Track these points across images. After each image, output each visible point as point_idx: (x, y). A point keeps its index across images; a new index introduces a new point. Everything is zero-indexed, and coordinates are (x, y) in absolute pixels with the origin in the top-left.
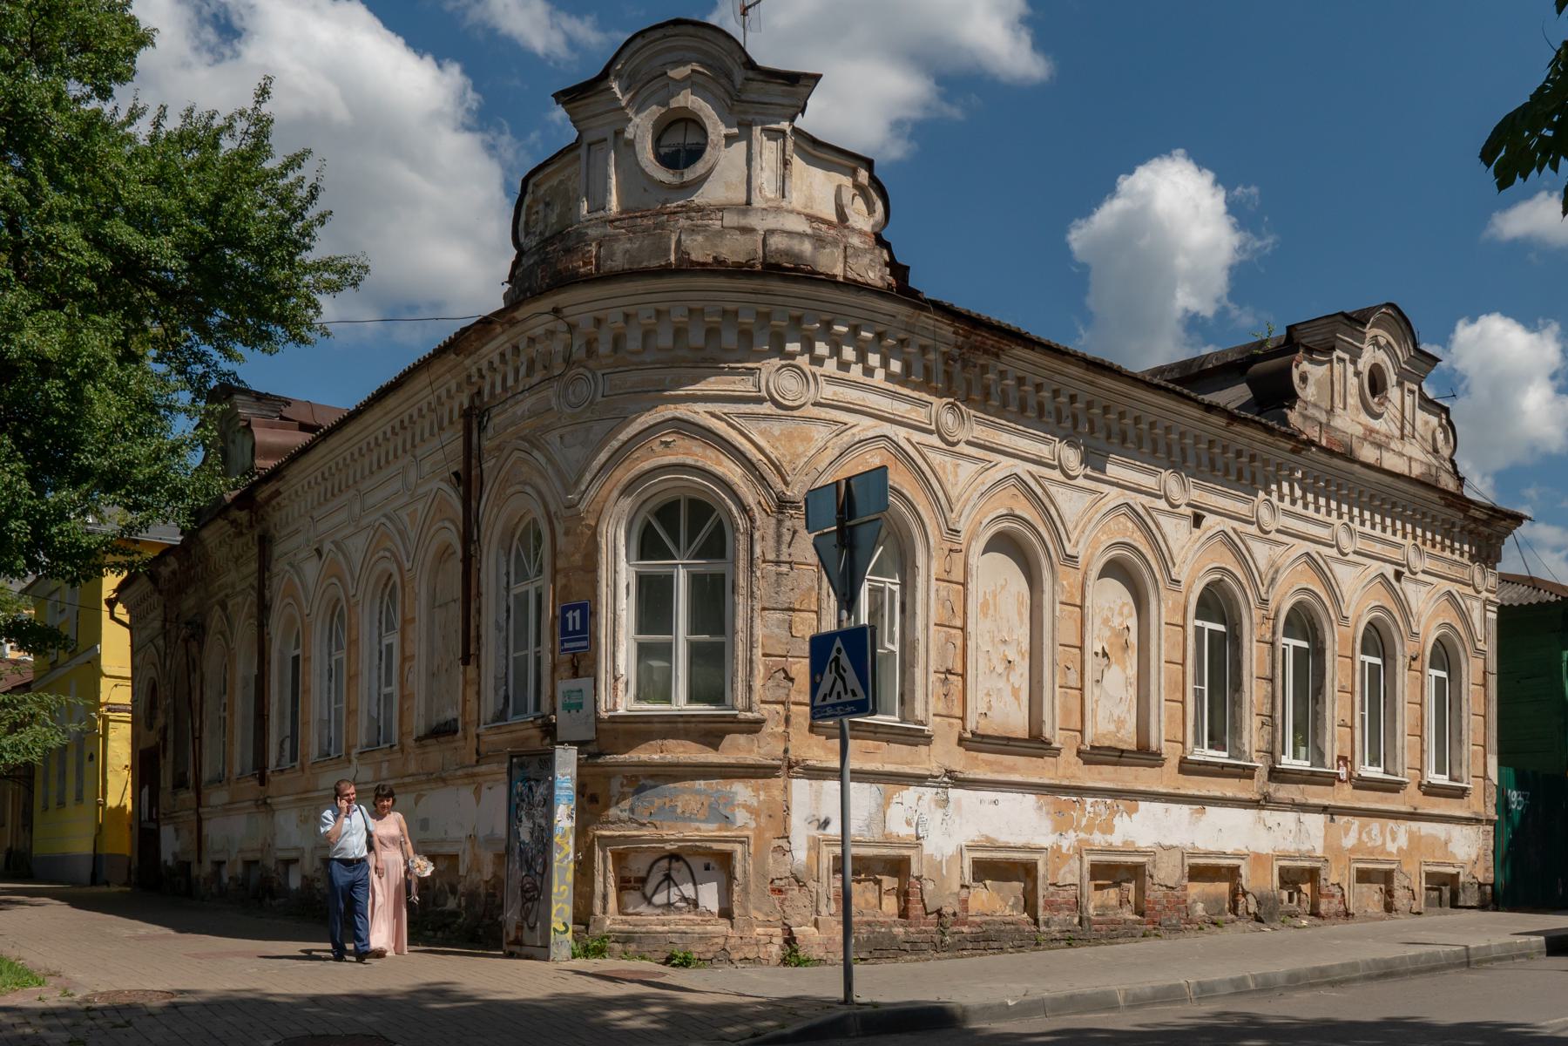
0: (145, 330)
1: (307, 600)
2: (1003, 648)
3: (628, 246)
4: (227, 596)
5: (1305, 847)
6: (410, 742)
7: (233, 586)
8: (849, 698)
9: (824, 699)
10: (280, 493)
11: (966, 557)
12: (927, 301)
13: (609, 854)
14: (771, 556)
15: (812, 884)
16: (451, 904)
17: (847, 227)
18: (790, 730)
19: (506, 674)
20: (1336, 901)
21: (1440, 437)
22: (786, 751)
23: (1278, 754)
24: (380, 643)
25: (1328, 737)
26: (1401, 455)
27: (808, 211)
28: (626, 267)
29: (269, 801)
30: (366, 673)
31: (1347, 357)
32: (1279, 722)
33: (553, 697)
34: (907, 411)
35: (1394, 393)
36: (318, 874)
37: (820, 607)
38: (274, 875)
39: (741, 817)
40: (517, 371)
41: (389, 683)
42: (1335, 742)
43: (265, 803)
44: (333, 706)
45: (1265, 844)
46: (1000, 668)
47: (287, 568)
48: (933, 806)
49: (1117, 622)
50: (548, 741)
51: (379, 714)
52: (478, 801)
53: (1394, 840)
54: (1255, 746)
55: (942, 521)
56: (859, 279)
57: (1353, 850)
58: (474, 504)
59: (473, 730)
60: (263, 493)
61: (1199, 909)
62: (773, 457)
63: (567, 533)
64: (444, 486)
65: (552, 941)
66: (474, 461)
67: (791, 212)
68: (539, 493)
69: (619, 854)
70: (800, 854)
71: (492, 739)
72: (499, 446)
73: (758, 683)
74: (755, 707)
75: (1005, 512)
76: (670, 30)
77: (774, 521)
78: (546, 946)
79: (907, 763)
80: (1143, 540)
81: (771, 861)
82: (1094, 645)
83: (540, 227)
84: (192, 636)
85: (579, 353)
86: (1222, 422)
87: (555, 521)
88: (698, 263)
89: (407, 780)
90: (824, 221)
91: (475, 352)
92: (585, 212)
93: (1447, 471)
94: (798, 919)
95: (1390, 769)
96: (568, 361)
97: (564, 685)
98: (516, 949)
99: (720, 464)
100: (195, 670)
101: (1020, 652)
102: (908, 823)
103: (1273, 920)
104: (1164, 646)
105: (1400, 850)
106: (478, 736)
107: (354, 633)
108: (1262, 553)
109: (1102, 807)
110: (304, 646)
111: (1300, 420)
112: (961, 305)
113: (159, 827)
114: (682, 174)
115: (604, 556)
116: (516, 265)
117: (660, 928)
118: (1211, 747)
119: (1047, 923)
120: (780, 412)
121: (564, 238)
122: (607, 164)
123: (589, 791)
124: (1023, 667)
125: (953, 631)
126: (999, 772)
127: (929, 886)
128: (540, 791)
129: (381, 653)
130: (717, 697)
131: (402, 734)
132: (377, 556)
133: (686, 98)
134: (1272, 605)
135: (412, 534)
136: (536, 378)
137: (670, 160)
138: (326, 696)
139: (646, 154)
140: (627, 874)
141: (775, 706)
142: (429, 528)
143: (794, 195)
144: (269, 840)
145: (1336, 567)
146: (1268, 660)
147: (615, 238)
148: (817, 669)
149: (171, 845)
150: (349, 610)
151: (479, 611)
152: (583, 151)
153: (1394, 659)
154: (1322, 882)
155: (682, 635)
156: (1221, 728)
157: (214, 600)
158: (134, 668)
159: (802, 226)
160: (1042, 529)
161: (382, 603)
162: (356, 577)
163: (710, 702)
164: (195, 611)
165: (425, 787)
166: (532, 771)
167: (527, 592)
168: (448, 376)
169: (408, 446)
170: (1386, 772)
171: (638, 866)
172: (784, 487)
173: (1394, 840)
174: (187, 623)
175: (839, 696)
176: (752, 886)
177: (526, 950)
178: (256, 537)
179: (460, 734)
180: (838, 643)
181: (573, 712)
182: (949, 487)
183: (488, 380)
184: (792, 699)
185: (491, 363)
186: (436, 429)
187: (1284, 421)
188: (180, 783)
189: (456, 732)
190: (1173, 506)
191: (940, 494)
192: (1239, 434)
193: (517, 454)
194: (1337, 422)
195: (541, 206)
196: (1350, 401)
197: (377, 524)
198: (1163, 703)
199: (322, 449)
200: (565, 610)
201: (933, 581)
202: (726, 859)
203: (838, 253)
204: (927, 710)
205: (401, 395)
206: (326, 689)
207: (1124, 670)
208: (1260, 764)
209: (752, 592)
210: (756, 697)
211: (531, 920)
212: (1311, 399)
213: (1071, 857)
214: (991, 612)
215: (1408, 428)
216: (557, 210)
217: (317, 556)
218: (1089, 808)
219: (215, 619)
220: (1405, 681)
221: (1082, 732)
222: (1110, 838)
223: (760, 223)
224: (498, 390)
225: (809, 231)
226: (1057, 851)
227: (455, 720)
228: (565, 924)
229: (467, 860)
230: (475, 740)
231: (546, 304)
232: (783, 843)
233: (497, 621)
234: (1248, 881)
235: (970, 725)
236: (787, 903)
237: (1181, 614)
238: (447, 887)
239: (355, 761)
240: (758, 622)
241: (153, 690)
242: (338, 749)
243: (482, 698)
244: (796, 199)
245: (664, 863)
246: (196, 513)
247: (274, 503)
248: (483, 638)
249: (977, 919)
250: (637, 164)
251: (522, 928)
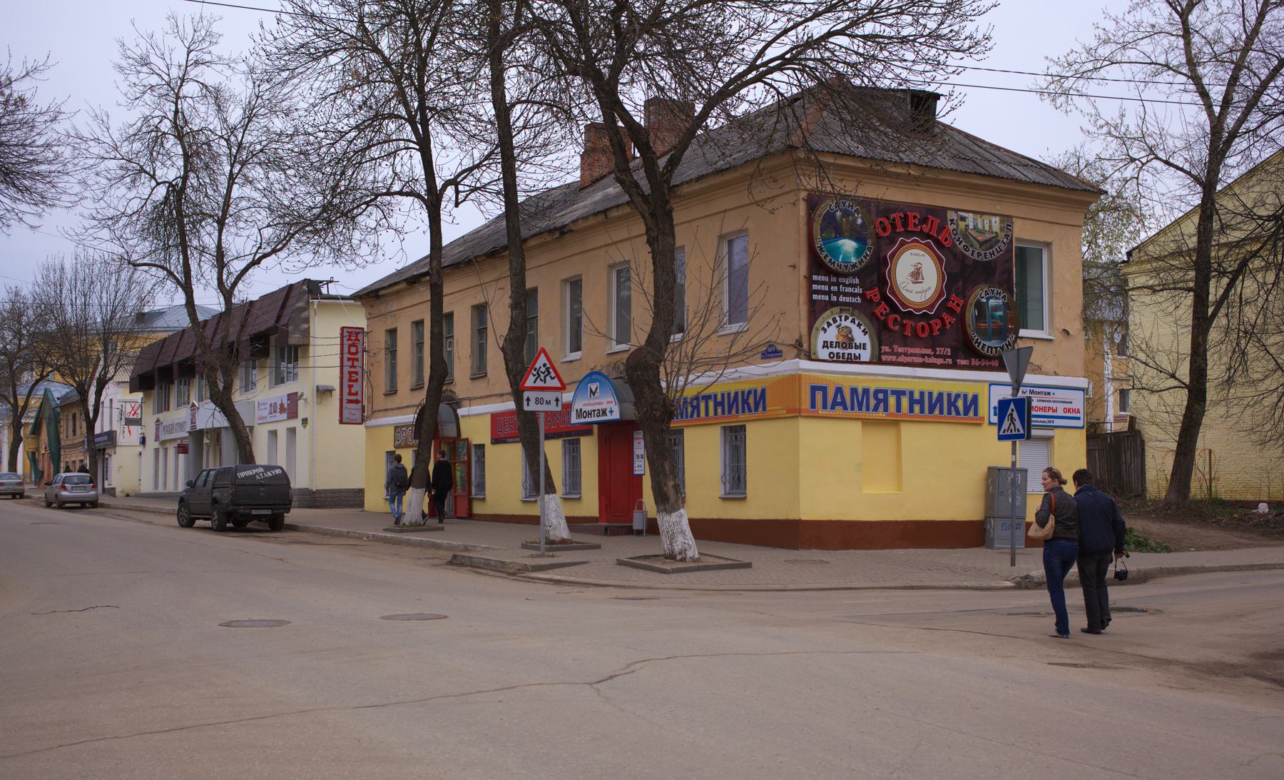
180: (1012, 406)
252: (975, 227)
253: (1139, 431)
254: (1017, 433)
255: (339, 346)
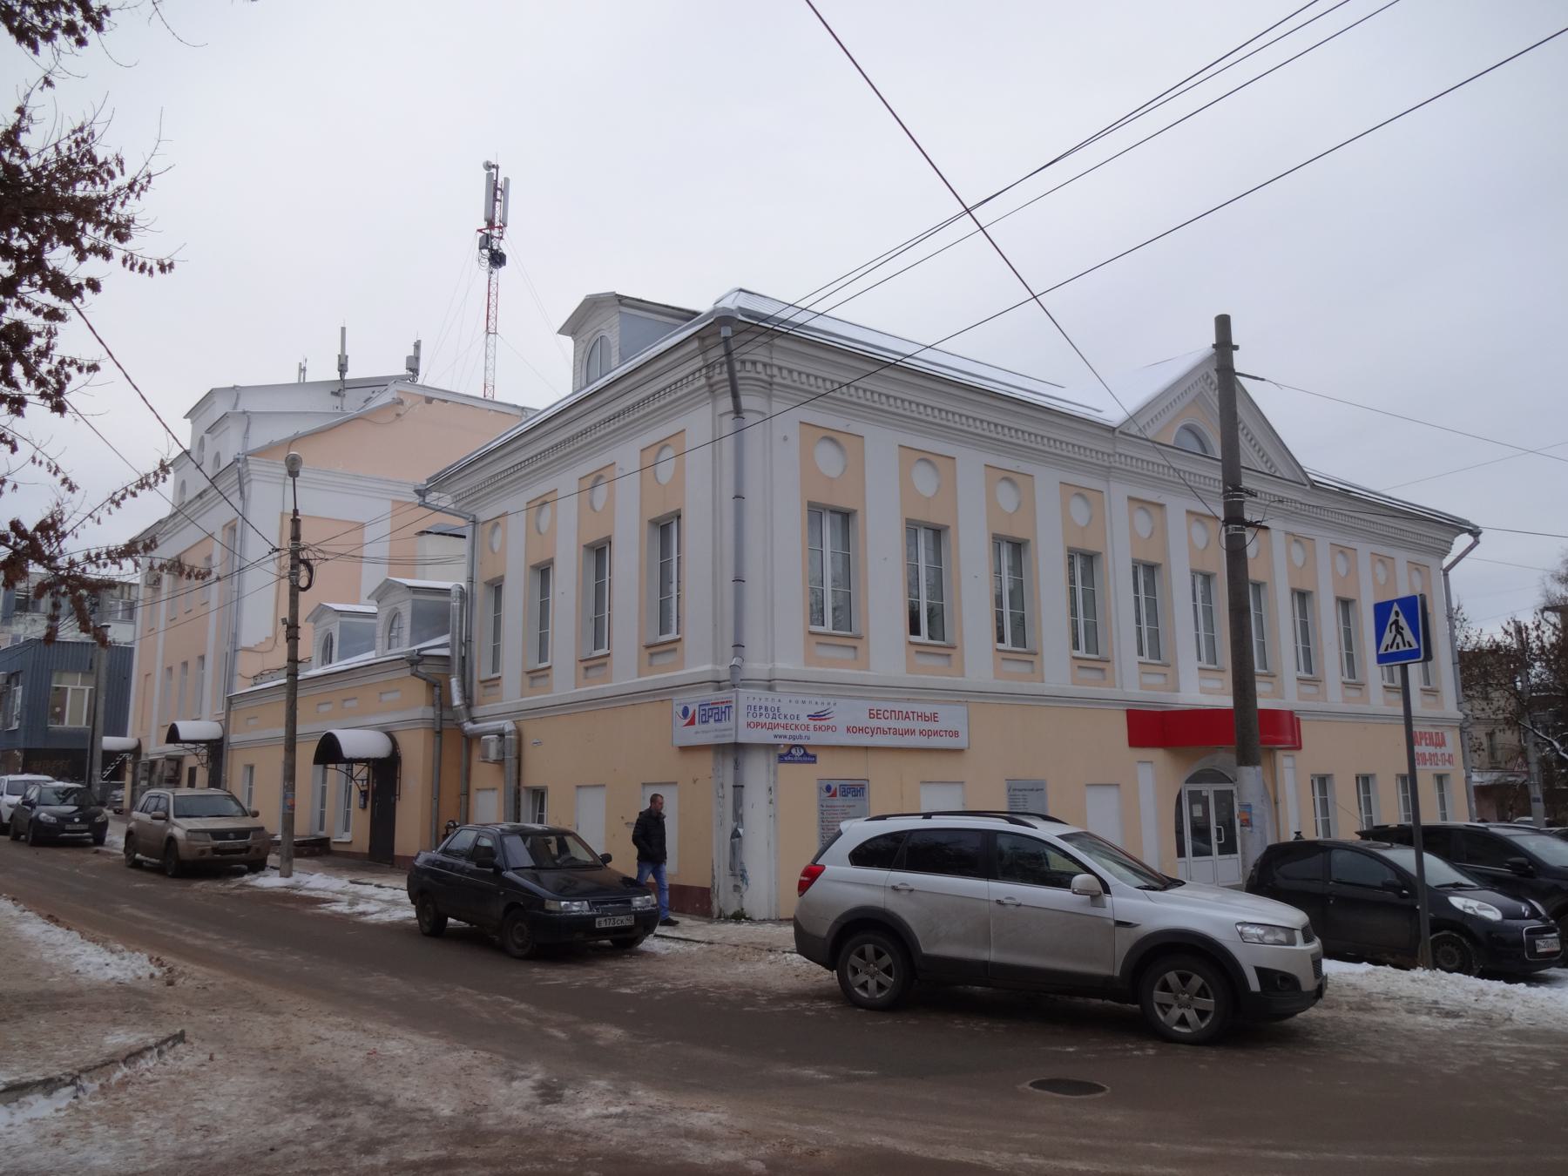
9: (1386, 650)
175: (1398, 647)
180: (1396, 607)
252: (716, 1145)
253: (937, 843)
254: (1407, 648)
255: (299, 731)
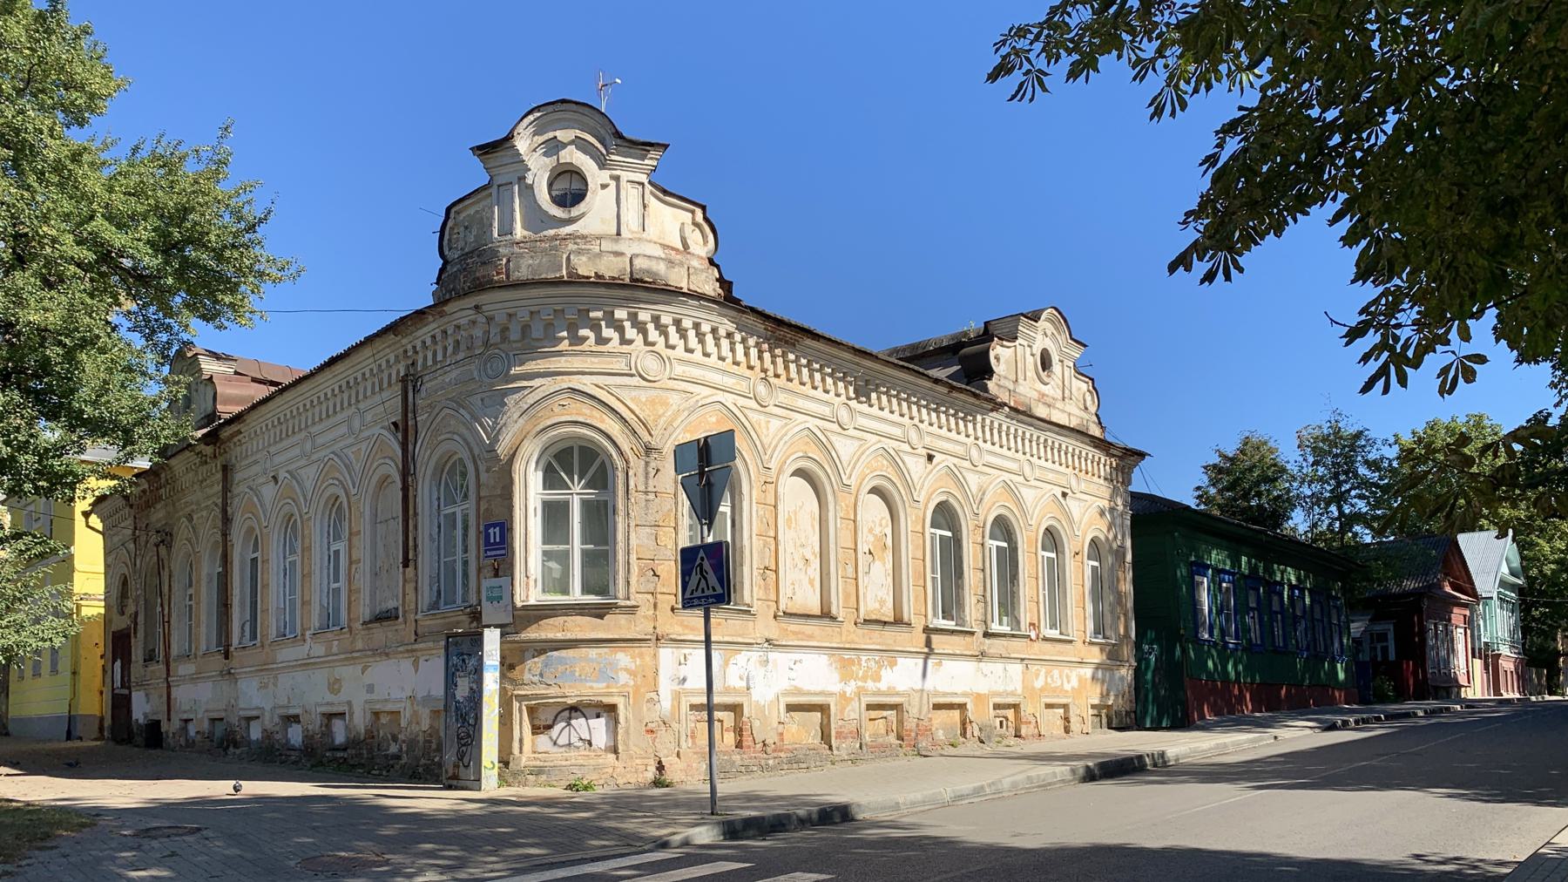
0: (119, 305)
1: (265, 516)
2: (801, 550)
3: (531, 262)
4: (193, 511)
5: (1010, 688)
6: (357, 626)
7: (198, 504)
8: (711, 592)
9: (692, 593)
10: (241, 433)
11: (776, 486)
12: (746, 307)
13: (524, 708)
14: (641, 488)
15: (675, 725)
16: (393, 749)
17: (689, 253)
18: (658, 613)
19: (438, 574)
20: (1032, 726)
21: (1088, 398)
22: (655, 628)
23: (989, 622)
24: (329, 549)
25: (1022, 609)
26: (1064, 411)
27: (660, 241)
28: (530, 277)
29: (232, 671)
30: (318, 572)
31: (1025, 343)
32: (989, 599)
33: (479, 592)
34: (734, 384)
35: (1056, 367)
36: (277, 728)
37: (676, 524)
38: (237, 729)
39: (623, 678)
40: (445, 349)
41: (337, 580)
42: (1026, 614)
43: (230, 673)
44: (288, 597)
45: (983, 687)
46: (801, 564)
47: (247, 490)
48: (758, 665)
49: (877, 530)
50: (475, 624)
51: (328, 604)
52: (416, 671)
53: (1069, 682)
54: (974, 618)
55: (759, 461)
56: (699, 291)
57: (1042, 690)
58: (410, 447)
59: (412, 617)
60: (225, 433)
61: (940, 735)
62: (641, 417)
63: (488, 471)
64: (385, 433)
65: (483, 775)
66: (410, 415)
67: (650, 241)
68: (465, 440)
69: (532, 708)
70: (666, 703)
71: (427, 623)
72: (430, 405)
73: (633, 580)
74: (632, 597)
75: (801, 454)
76: (559, 107)
77: (643, 463)
78: (479, 780)
79: (740, 636)
80: (893, 472)
81: (645, 709)
82: (863, 547)
83: (461, 244)
84: (162, 541)
85: (495, 338)
86: (945, 390)
87: (479, 463)
88: (584, 277)
89: (355, 655)
90: (673, 249)
91: (411, 334)
92: (496, 236)
93: (1094, 422)
94: (666, 751)
95: (1063, 631)
96: (487, 344)
97: (487, 583)
98: (454, 782)
99: (603, 421)
100: (163, 568)
101: (814, 553)
102: (741, 678)
103: (990, 742)
104: (909, 550)
105: (1073, 688)
106: (416, 621)
107: (307, 541)
108: (973, 481)
109: (873, 663)
110: (262, 550)
111: (996, 387)
112: (769, 311)
113: (130, 693)
114: (570, 211)
115: (518, 487)
116: (442, 271)
117: (564, 763)
118: (943, 618)
119: (838, 749)
120: (645, 383)
121: (483, 254)
122: (513, 201)
123: (508, 662)
124: (816, 563)
125: (768, 539)
126: (802, 640)
127: (756, 724)
128: (472, 663)
129: (329, 556)
130: (603, 591)
131: (350, 620)
132: (324, 485)
133: (571, 154)
134: (981, 518)
135: (357, 467)
136: (461, 355)
137: (562, 201)
138: (282, 589)
139: (543, 196)
140: (537, 722)
141: (646, 595)
142: (371, 464)
143: (652, 229)
144: (233, 701)
145: (1022, 489)
146: (980, 556)
147: (521, 256)
148: (686, 574)
149: (141, 709)
150: (302, 522)
151: (416, 527)
152: (494, 190)
153: (1063, 553)
154: (1022, 713)
155: (577, 545)
156: (951, 604)
157: (181, 513)
158: (107, 566)
159: (658, 252)
160: (827, 467)
161: (330, 518)
162: (308, 498)
163: (597, 594)
164: (163, 522)
165: (371, 660)
166: (465, 648)
167: (454, 513)
168: (388, 350)
169: (353, 401)
170: (1061, 634)
171: (545, 717)
172: (650, 438)
173: (1069, 682)
174: (158, 532)
175: (703, 591)
176: (632, 729)
177: (461, 783)
178: (219, 467)
179: (401, 619)
180: (702, 554)
181: (495, 602)
182: (763, 438)
183: (421, 355)
184: (659, 591)
185: (424, 342)
186: (377, 389)
187: (986, 390)
188: (150, 658)
189: (397, 618)
190: (913, 449)
191: (758, 443)
192: (956, 398)
193: (448, 411)
194: (1020, 389)
195: (462, 229)
196: (1028, 374)
197: (326, 459)
198: (911, 587)
199: (279, 400)
200: (487, 527)
201: (754, 504)
202: (612, 709)
203: (684, 272)
204: (752, 596)
205: (347, 363)
206: (282, 585)
207: (884, 564)
208: (979, 631)
209: (628, 514)
210: (632, 590)
211: (466, 760)
212: (1002, 373)
213: (852, 699)
214: (793, 525)
215: (1067, 392)
216: (474, 232)
217: (272, 483)
218: (864, 664)
219: (182, 532)
220: (1071, 565)
221: (857, 610)
222: (878, 685)
223: (629, 249)
224: (430, 363)
225: (663, 256)
226: (843, 695)
227: (397, 609)
228: (492, 762)
229: (408, 715)
230: (414, 624)
231: (470, 302)
232: (653, 695)
233: (431, 534)
234: (973, 713)
235: (782, 607)
236: (657, 740)
237: (921, 524)
238: (390, 737)
239: (309, 640)
240: (633, 535)
241: (125, 583)
242: (293, 630)
243: (420, 593)
244: (652, 232)
245: (566, 714)
246: (163, 452)
247: (235, 439)
248: (420, 546)
249: (790, 747)
250: (536, 202)
251: (458, 767)
